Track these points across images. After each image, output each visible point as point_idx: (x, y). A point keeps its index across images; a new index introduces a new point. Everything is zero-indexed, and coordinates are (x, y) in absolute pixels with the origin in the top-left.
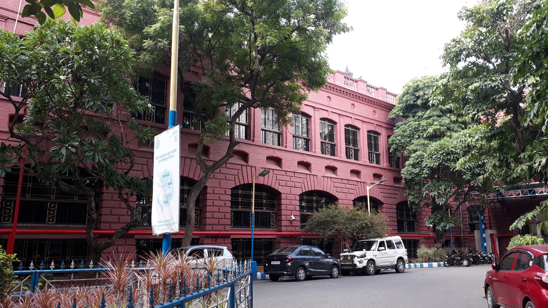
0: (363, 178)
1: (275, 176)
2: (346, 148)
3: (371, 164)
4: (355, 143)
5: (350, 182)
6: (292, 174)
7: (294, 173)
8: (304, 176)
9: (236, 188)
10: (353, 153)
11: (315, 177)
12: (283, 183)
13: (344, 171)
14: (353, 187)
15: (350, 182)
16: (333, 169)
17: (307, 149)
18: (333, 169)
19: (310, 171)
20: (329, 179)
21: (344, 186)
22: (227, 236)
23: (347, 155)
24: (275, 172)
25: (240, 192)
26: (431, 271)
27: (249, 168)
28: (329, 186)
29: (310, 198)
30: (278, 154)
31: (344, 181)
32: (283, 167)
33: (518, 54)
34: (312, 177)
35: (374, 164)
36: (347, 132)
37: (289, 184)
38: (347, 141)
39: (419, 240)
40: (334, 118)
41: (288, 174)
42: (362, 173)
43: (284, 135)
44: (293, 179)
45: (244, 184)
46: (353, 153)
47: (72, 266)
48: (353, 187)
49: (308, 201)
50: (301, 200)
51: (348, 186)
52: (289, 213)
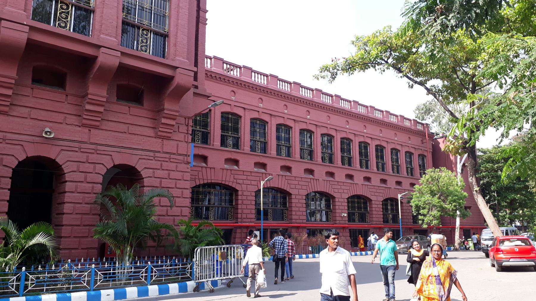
0: (356, 180)
1: (232, 176)
2: (377, 162)
3: (394, 174)
4: (366, 156)
5: (303, 180)
6: (300, 179)
10: (348, 161)
12: (336, 191)
16: (331, 174)
18: (331, 174)
19: (386, 185)
23: (322, 160)
24: (331, 183)
25: (201, 189)
26: (301, 260)
29: (353, 200)
30: (288, 164)
31: (375, 188)
32: (209, 163)
34: (208, 170)
35: (364, 169)
37: (298, 187)
38: (342, 150)
39: (369, 230)
41: (297, 179)
42: (335, 175)
47: (32, 269)
48: (382, 191)
49: (352, 202)
50: (348, 202)
51: (378, 191)
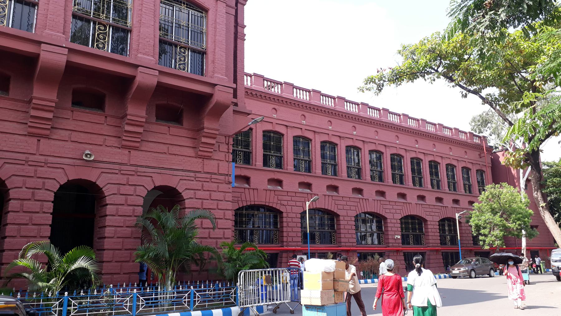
1: (276, 197)
3: (450, 192)
6: (348, 199)
7: (295, 193)
8: (440, 208)
9: (406, 217)
11: (255, 191)
13: (431, 199)
14: (438, 211)
15: (351, 200)
17: (359, 178)
20: (379, 202)
21: (431, 210)
22: (355, 251)
23: (393, 180)
27: (364, 200)
28: (379, 208)
29: (406, 221)
32: (252, 184)
33: (532, 22)
34: (251, 191)
36: (392, 160)
37: (346, 207)
38: (393, 167)
40: (382, 149)
41: (344, 199)
43: (285, 158)
44: (349, 203)
45: (405, 217)
46: (418, 179)
48: (438, 211)
49: (405, 223)
50: (401, 223)
51: (434, 210)
52: (393, 233)
